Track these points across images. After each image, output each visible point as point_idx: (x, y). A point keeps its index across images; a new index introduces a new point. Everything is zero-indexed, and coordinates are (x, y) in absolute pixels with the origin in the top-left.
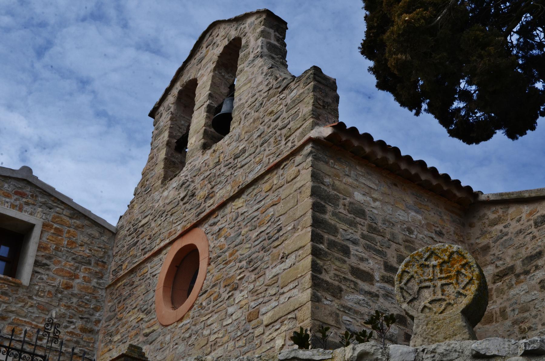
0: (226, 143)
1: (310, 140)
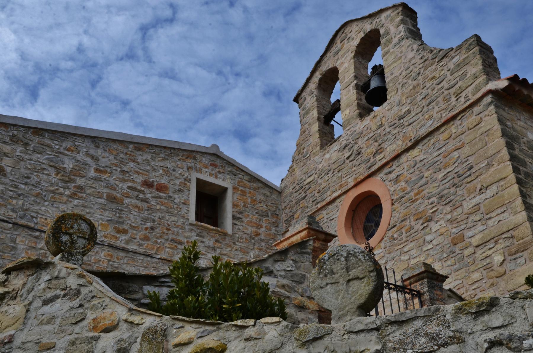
0: (386, 109)
1: (490, 92)
